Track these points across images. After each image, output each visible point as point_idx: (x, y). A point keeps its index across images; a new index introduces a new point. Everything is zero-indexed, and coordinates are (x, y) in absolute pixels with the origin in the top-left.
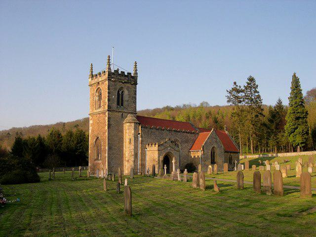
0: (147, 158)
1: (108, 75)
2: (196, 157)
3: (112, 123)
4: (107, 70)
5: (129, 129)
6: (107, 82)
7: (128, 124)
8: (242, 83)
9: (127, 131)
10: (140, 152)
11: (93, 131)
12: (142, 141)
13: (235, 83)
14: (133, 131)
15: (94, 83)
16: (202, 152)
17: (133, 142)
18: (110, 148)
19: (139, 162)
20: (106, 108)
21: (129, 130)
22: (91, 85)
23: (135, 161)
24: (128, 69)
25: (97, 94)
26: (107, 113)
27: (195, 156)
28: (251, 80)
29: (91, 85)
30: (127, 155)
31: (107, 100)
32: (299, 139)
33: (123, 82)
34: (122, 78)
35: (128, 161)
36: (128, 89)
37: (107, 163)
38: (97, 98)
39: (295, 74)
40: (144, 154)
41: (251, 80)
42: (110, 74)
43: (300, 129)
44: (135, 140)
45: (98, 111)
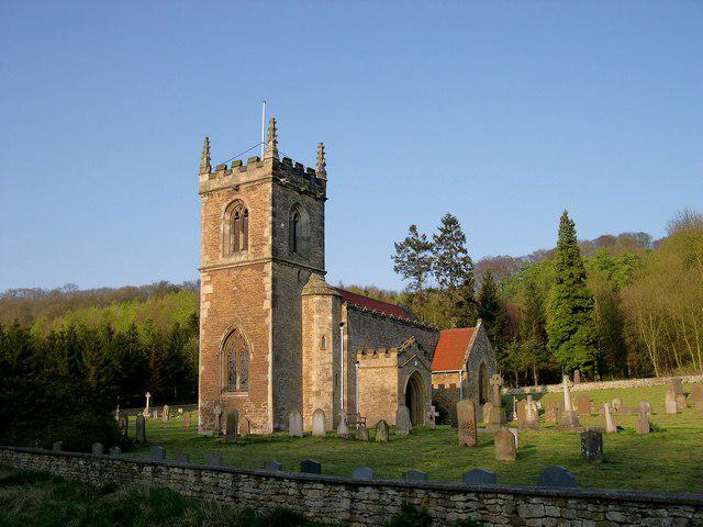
0: (361, 387)
1: (274, 168)
2: (447, 386)
3: (281, 292)
4: (266, 154)
5: (319, 311)
6: (269, 186)
7: (318, 298)
8: (430, 229)
9: (316, 316)
10: (344, 370)
11: (213, 313)
12: (349, 342)
13: (413, 229)
14: (331, 318)
15: (217, 186)
16: (465, 374)
17: (329, 344)
18: (276, 359)
19: (344, 397)
20: (267, 252)
21: (317, 319)
22: (207, 193)
23: (335, 395)
24: (310, 162)
25: (228, 217)
26: (269, 268)
27: (442, 386)
28: (450, 222)
29: (207, 193)
30: (314, 378)
31: (267, 232)
32: (581, 355)
33: (303, 189)
35: (318, 394)
36: (309, 208)
37: (270, 398)
38: (228, 227)
39: (565, 214)
40: (352, 377)
41: (450, 222)
42: (276, 166)
43: (583, 333)
44: (334, 338)
45: (235, 259)
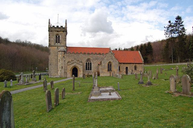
8: (173, 21)
13: (170, 22)
28: (179, 18)
34: (57, 29)
41: (179, 18)
